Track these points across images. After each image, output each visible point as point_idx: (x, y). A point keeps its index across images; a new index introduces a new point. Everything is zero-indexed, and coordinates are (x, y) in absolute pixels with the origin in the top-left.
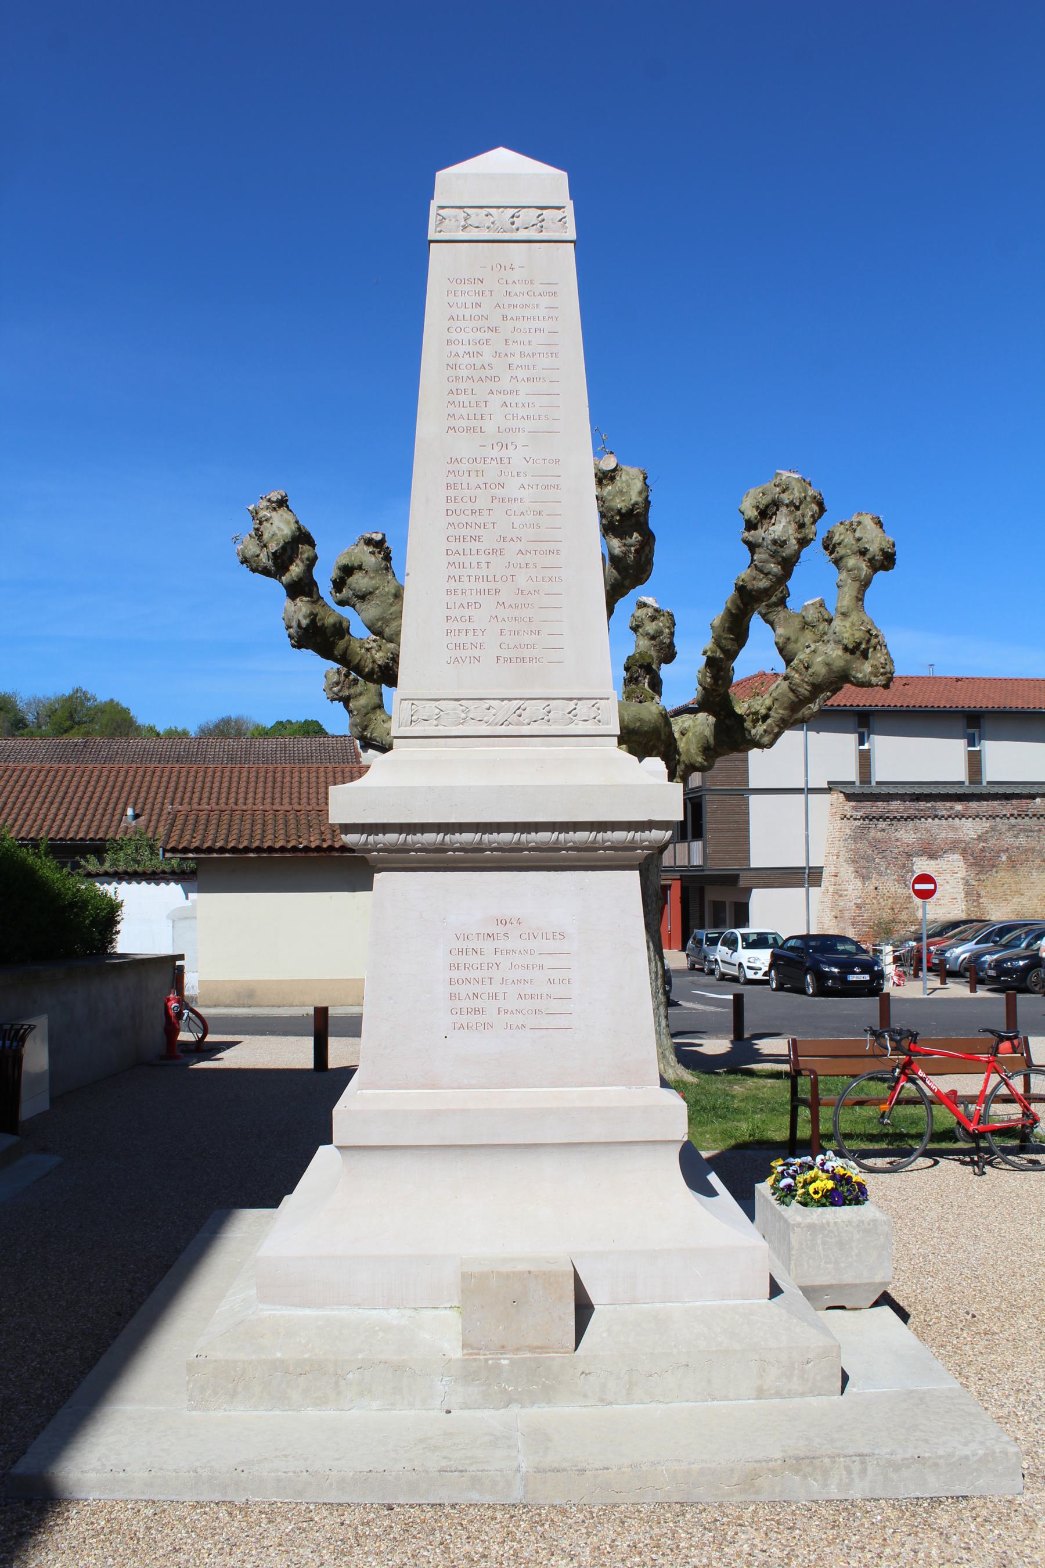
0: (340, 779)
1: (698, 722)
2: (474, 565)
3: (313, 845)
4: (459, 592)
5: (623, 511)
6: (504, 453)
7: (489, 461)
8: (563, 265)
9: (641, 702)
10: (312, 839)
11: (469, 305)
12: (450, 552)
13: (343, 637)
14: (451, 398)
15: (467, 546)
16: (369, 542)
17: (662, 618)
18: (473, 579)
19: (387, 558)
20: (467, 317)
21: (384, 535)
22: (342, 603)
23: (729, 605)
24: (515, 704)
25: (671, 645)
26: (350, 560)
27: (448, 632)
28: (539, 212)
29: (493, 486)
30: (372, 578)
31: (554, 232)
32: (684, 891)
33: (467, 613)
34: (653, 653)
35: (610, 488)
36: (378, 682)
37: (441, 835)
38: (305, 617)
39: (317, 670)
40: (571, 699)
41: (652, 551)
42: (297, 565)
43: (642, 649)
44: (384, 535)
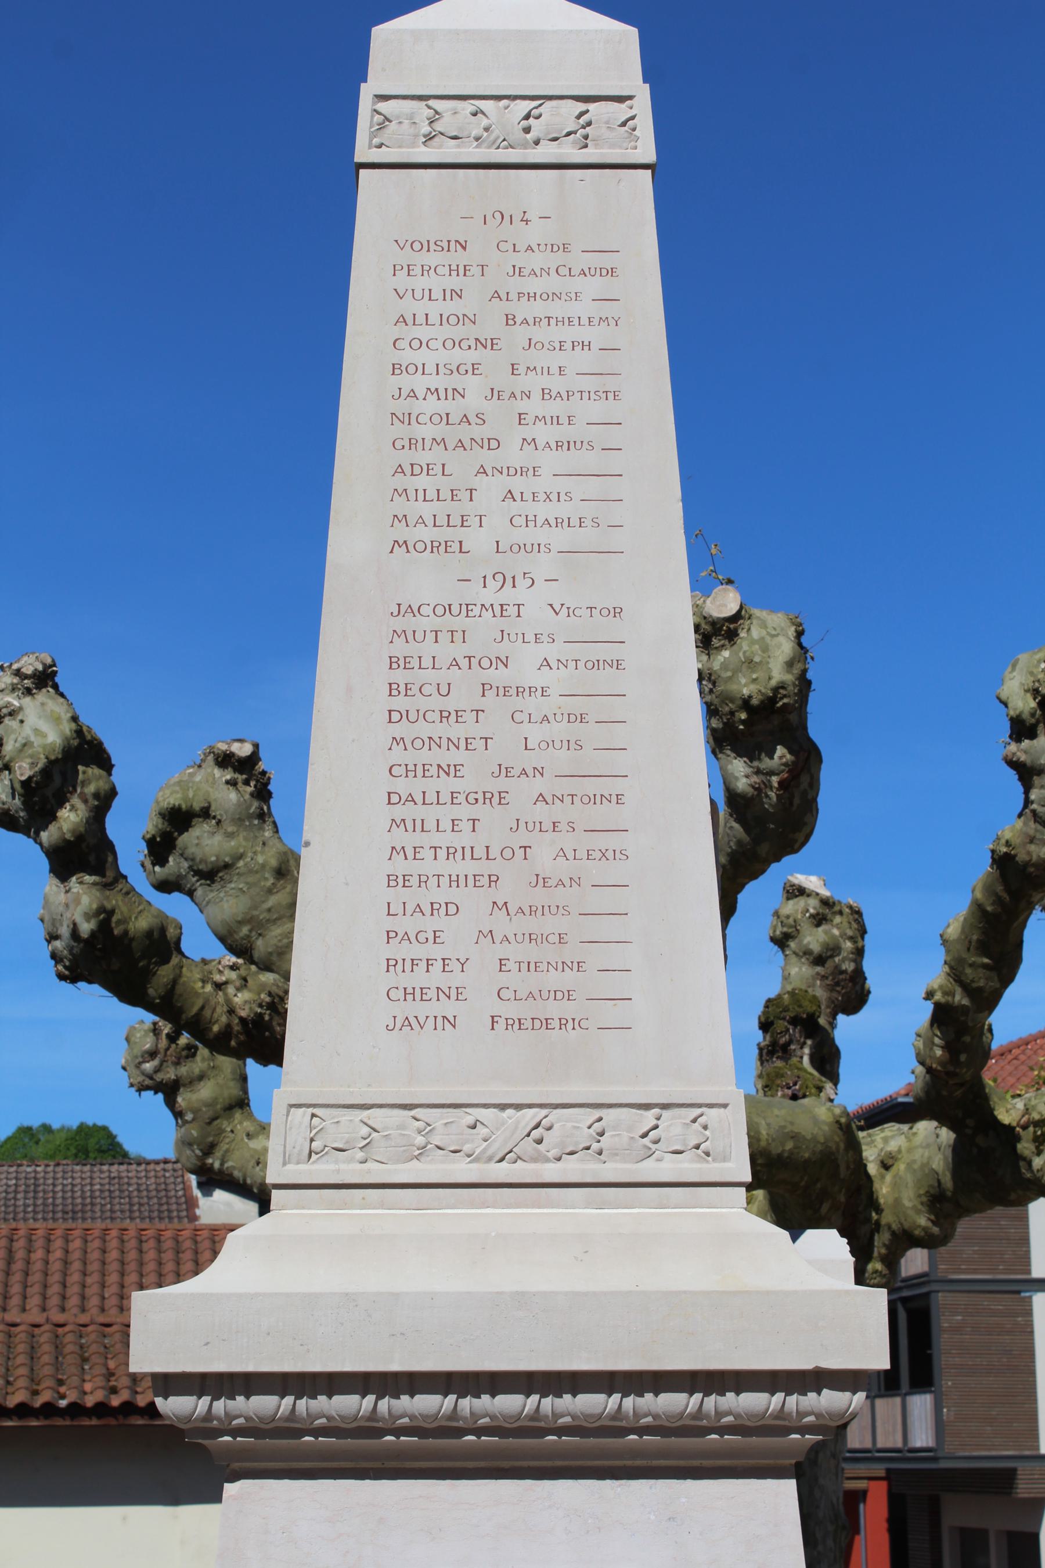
0: (152, 1278)
1: (919, 1140)
2: (446, 824)
3: (90, 1401)
4: (414, 881)
5: (755, 702)
6: (508, 595)
7: (476, 610)
8: (631, 209)
9: (794, 1097)
10: (88, 1387)
11: (437, 294)
12: (395, 798)
13: (166, 960)
14: (400, 482)
15: (432, 785)
16: (225, 760)
17: (838, 919)
18: (442, 854)
19: (263, 794)
20: (434, 318)
21: (256, 746)
22: (165, 886)
23: (979, 895)
24: (530, 1116)
25: (858, 976)
26: (185, 798)
27: (390, 964)
28: (582, 107)
29: (485, 663)
30: (230, 835)
31: (612, 146)
32: (897, 1505)
33: (430, 924)
34: (820, 992)
35: (726, 654)
36: (240, 1054)
37: (370, 1399)
38: (87, 917)
39: (108, 1026)
40: (647, 1107)
41: (814, 784)
42: (73, 808)
43: (796, 983)
44: (256, 746)
